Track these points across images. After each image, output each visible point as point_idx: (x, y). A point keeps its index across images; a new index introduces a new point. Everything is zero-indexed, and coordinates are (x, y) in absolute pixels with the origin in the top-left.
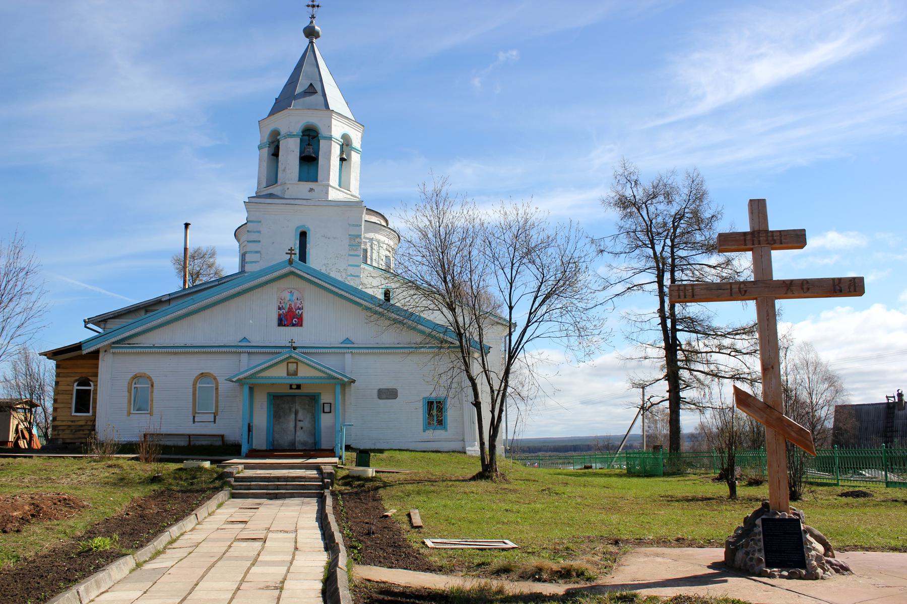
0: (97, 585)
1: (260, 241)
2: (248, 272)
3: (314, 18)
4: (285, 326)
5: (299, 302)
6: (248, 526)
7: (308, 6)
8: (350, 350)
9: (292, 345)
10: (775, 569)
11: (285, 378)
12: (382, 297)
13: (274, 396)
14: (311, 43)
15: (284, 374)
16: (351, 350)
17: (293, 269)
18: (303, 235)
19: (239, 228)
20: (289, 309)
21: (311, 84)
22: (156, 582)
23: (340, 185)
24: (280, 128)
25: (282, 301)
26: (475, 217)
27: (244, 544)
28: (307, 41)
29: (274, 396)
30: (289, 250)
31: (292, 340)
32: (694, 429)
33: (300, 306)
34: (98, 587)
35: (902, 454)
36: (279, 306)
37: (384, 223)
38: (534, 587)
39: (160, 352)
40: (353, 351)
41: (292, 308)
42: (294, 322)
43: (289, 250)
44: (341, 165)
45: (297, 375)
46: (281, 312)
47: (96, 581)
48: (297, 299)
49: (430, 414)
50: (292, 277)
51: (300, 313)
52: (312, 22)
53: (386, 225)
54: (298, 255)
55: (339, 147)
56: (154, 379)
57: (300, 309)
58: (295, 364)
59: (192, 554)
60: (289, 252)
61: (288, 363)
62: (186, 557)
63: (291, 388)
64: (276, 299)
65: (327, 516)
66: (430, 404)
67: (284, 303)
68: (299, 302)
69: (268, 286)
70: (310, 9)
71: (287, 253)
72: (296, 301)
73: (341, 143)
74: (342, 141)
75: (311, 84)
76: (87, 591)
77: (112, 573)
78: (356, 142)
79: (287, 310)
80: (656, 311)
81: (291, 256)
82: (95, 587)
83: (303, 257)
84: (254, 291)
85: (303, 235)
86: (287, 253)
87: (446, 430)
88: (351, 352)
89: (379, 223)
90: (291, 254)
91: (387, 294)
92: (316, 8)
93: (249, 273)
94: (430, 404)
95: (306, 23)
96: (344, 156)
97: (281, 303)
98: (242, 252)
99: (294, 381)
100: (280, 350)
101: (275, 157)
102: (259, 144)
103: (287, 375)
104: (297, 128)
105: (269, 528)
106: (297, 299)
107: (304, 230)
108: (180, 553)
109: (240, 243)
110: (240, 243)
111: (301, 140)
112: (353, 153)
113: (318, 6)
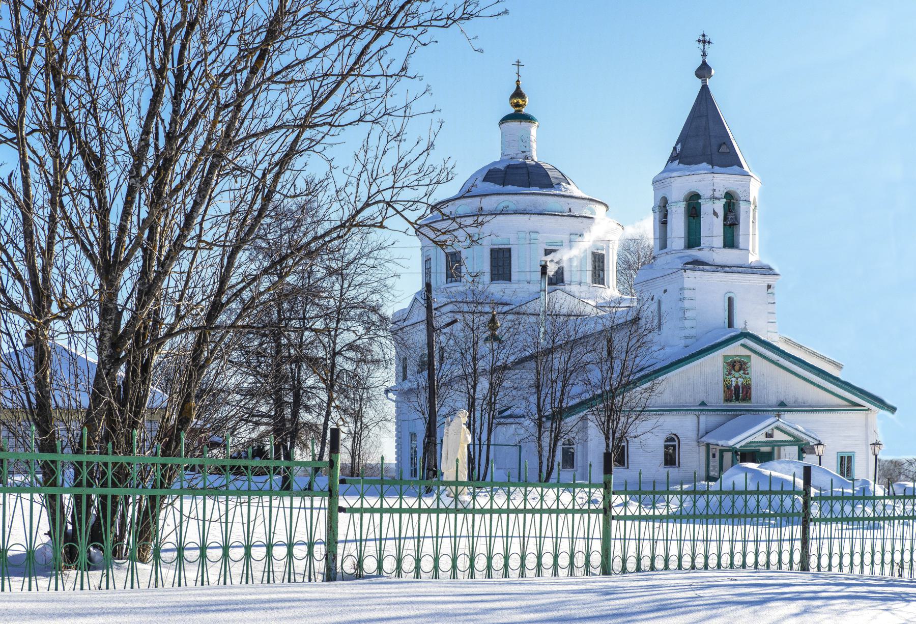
7: (699, 41)
14: (704, 82)
18: (730, 301)
70: (701, 45)
85: (730, 301)
94: (842, 457)
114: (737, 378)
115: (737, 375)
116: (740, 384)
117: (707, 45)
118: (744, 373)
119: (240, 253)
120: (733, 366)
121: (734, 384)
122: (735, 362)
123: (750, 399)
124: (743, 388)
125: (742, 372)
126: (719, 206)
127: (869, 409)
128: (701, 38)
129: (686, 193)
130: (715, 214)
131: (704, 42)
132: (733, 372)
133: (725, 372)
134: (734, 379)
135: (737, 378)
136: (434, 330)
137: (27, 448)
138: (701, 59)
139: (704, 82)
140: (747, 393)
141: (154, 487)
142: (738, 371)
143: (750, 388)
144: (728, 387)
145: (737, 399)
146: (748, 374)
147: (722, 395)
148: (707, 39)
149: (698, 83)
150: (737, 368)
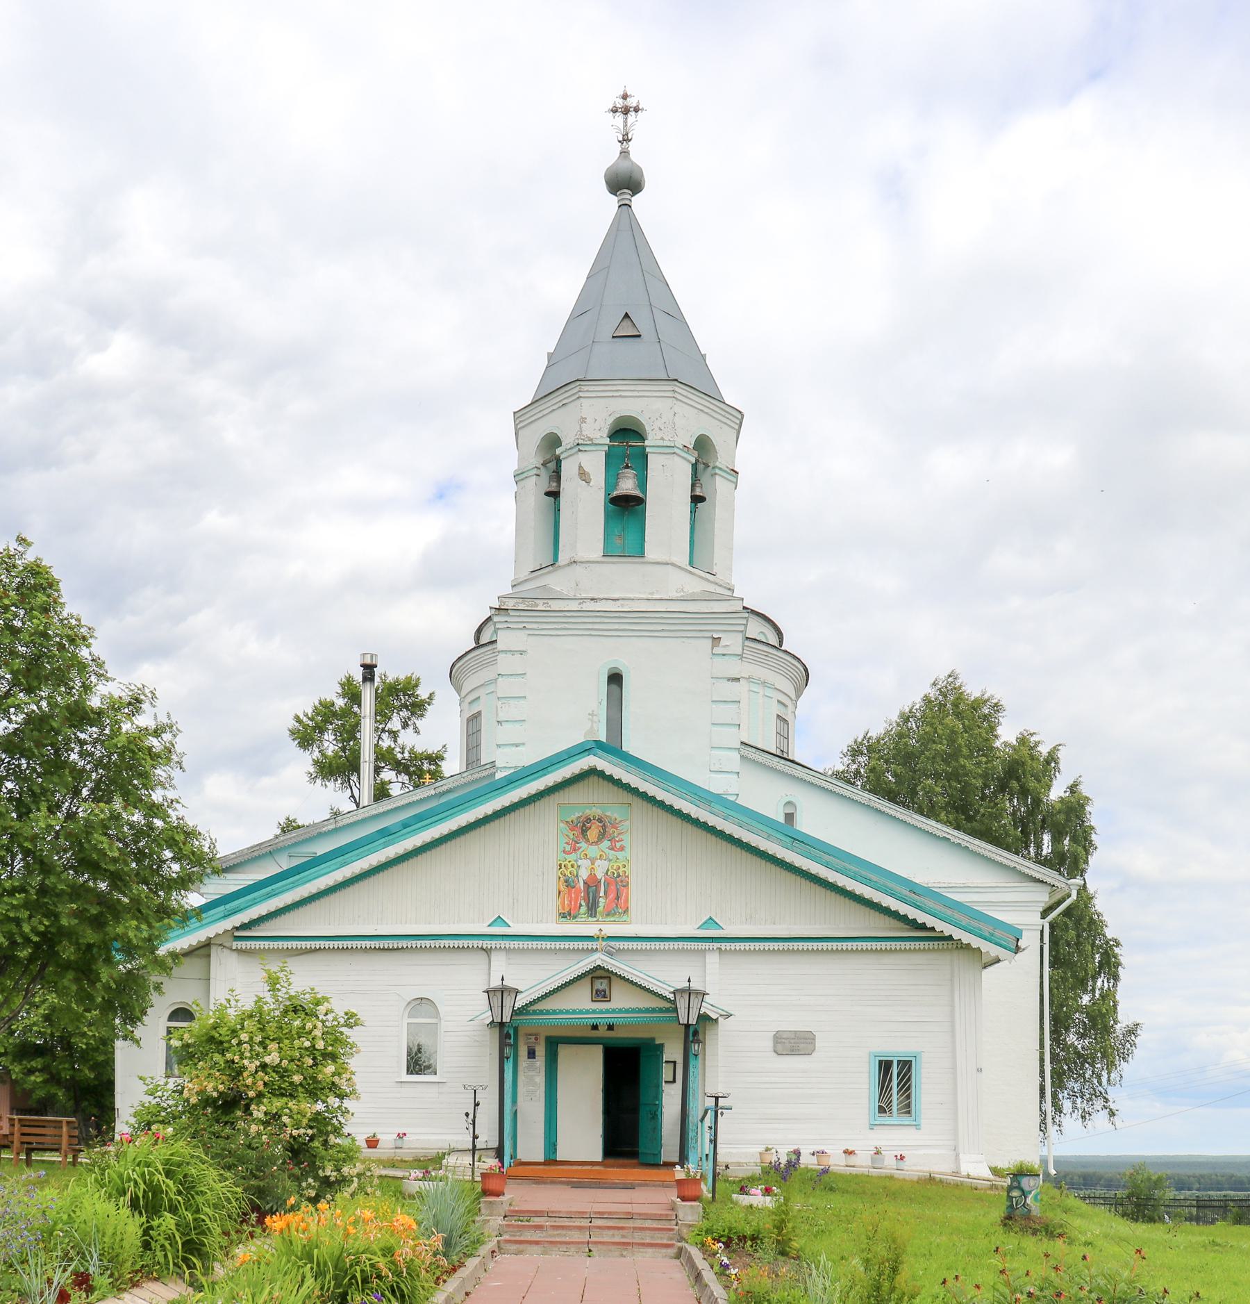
1: (525, 697)
3: (628, 140)
7: (614, 111)
8: (717, 945)
12: (781, 819)
14: (625, 206)
16: (718, 945)
19: (460, 658)
21: (627, 316)
23: (691, 564)
35: (227, 1183)
37: (773, 640)
39: (403, 948)
40: (723, 946)
44: (693, 512)
49: (884, 1086)
52: (625, 153)
53: (777, 645)
56: (775, 1055)
70: (619, 118)
75: (627, 316)
80: (605, 435)
87: (917, 1126)
92: (633, 113)
94: (885, 1067)
95: (611, 156)
96: (698, 492)
98: (467, 715)
102: (517, 468)
104: (599, 431)
109: (463, 694)
110: (463, 694)
111: (607, 455)
113: (636, 110)
114: (593, 861)
115: (593, 851)
116: (600, 875)
117: (632, 117)
118: (612, 849)
119: (196, 905)
120: (584, 831)
121: (584, 874)
122: (588, 820)
123: (626, 911)
124: (607, 884)
125: (606, 843)
126: (595, 463)
127: (950, 938)
128: (620, 103)
129: (1105, 918)
130: (584, 475)
131: (626, 111)
132: (583, 845)
133: (562, 845)
134: (584, 863)
135: (593, 861)
136: (551, 1161)
137: (9, 1181)
138: (618, 147)
139: (625, 206)
140: (618, 898)
141: (72, 1247)
142: (596, 843)
143: (626, 886)
144: (569, 883)
145: (592, 910)
146: (622, 849)
147: (552, 904)
148: (632, 102)
149: (611, 203)
150: (593, 834)
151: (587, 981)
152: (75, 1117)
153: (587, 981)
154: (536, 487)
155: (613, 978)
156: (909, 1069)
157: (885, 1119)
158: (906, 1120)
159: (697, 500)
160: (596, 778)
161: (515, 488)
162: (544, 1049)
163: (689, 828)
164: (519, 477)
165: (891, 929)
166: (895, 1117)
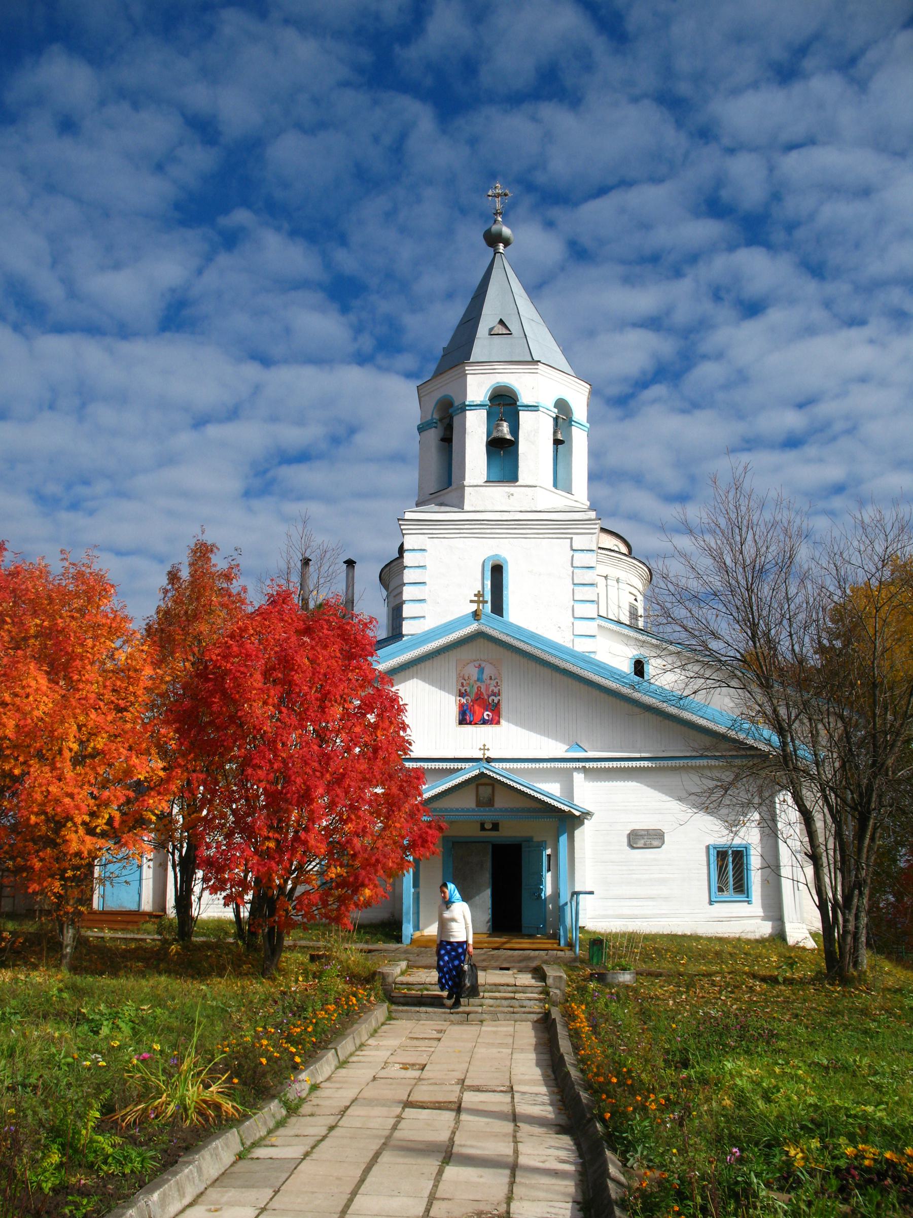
0: (179, 1190)
2: (407, 635)
4: (470, 723)
5: (493, 683)
6: (426, 1074)
9: (484, 754)
10: (836, 934)
11: (473, 810)
13: (453, 843)
15: (473, 805)
16: (583, 764)
17: (485, 629)
20: (477, 694)
22: (279, 1191)
23: (555, 485)
24: (451, 394)
25: (465, 683)
26: (786, 525)
27: (425, 1114)
28: (492, 249)
29: (453, 843)
30: (475, 595)
31: (484, 745)
32: (407, 721)
33: (496, 690)
34: (182, 1195)
36: (460, 691)
37: (624, 550)
38: (95, 560)
40: (587, 765)
41: (482, 694)
42: (487, 718)
43: (475, 595)
44: (556, 451)
45: (493, 805)
46: (463, 701)
47: (177, 1183)
48: (491, 679)
49: (722, 870)
50: (481, 641)
51: (496, 701)
54: (489, 604)
55: (552, 419)
57: (494, 694)
58: (489, 789)
59: (337, 1129)
60: (476, 599)
61: (478, 786)
62: (324, 1138)
63: (483, 828)
64: (455, 680)
65: (564, 1059)
66: (722, 855)
67: (469, 684)
68: (493, 683)
69: (442, 656)
71: (472, 601)
72: (488, 682)
73: (554, 415)
74: (556, 411)
76: (163, 1202)
77: (204, 1166)
78: (580, 412)
79: (473, 696)
81: (478, 606)
82: (176, 1195)
83: (498, 607)
84: (419, 666)
86: (472, 601)
87: (749, 902)
88: (584, 767)
89: (617, 549)
90: (478, 602)
91: (639, 667)
93: (644, 541)
94: (722, 855)
96: (560, 437)
97: (463, 685)
98: (392, 605)
99: (488, 816)
100: (463, 765)
101: (446, 444)
103: (477, 805)
105: (463, 1081)
106: (491, 679)
107: (498, 563)
108: (316, 1128)
112: (575, 430)
136: (435, 1198)
151: (473, 786)
152: (408, 770)
153: (473, 786)
154: (433, 435)
155: (497, 786)
156: (742, 857)
157: (726, 896)
158: (742, 897)
159: (557, 442)
160: (482, 640)
161: (418, 438)
162: (441, 870)
163: (557, 676)
164: (421, 429)
165: (682, 751)
166: (729, 894)
